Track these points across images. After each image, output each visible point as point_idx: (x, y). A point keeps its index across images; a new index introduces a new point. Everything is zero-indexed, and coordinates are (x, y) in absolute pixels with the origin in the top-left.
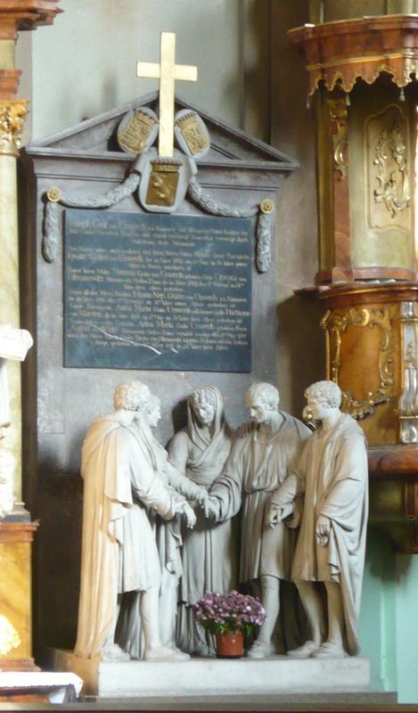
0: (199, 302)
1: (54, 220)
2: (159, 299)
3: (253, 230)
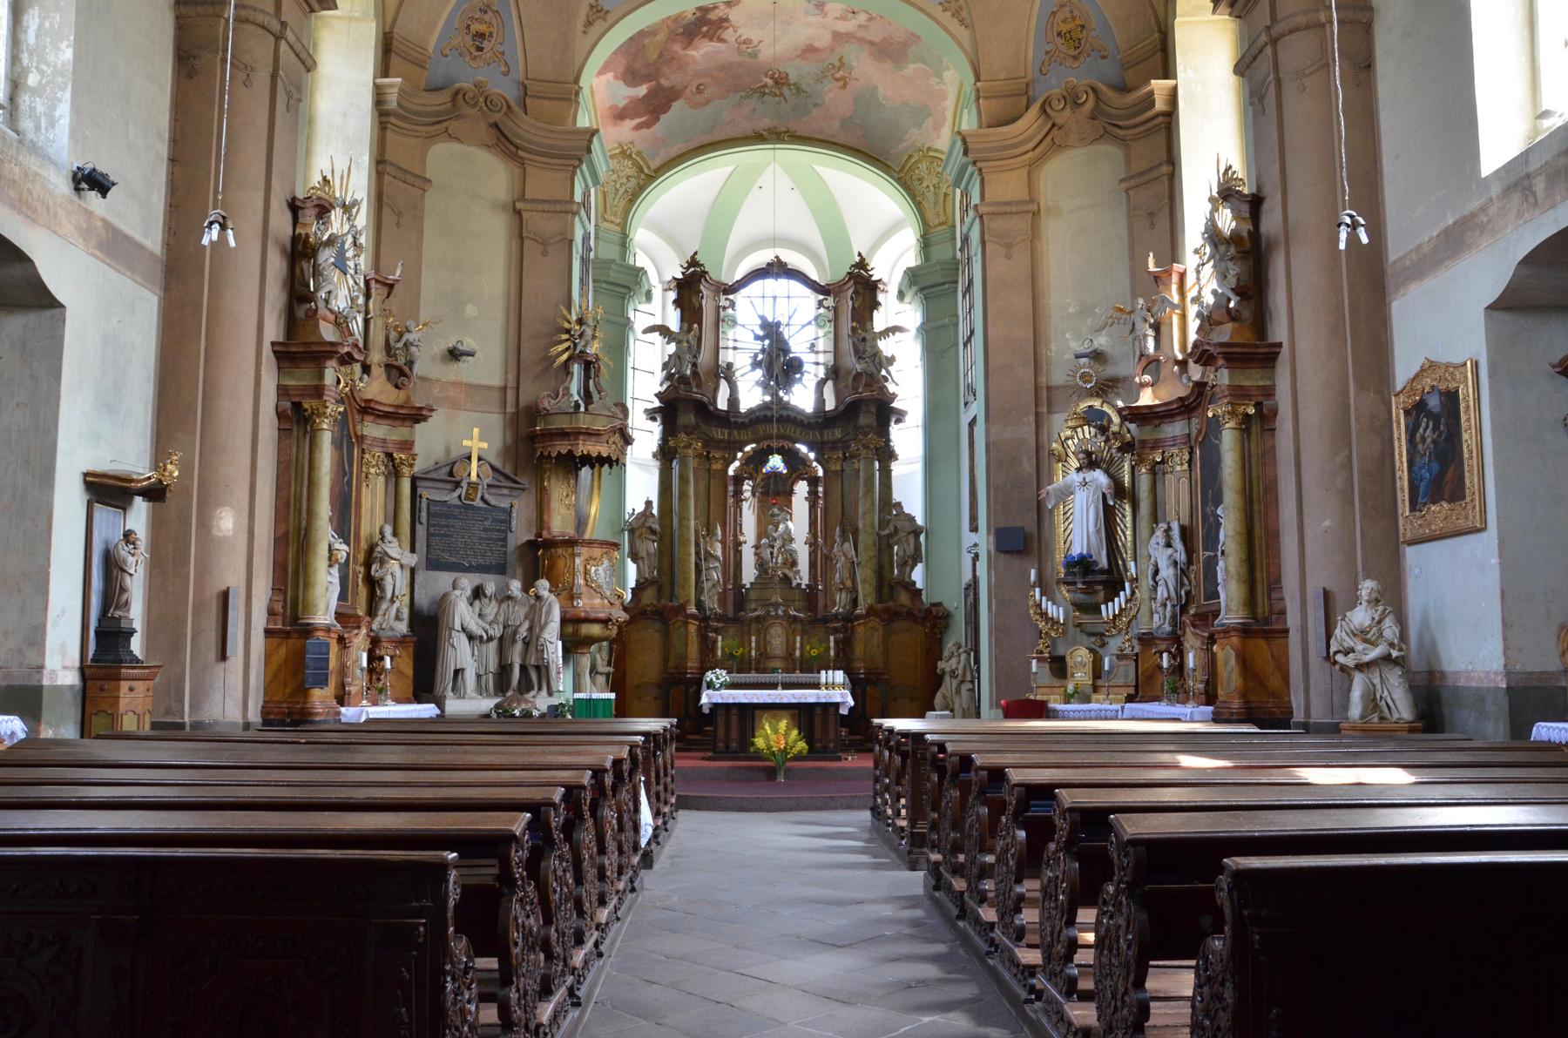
1: (424, 505)
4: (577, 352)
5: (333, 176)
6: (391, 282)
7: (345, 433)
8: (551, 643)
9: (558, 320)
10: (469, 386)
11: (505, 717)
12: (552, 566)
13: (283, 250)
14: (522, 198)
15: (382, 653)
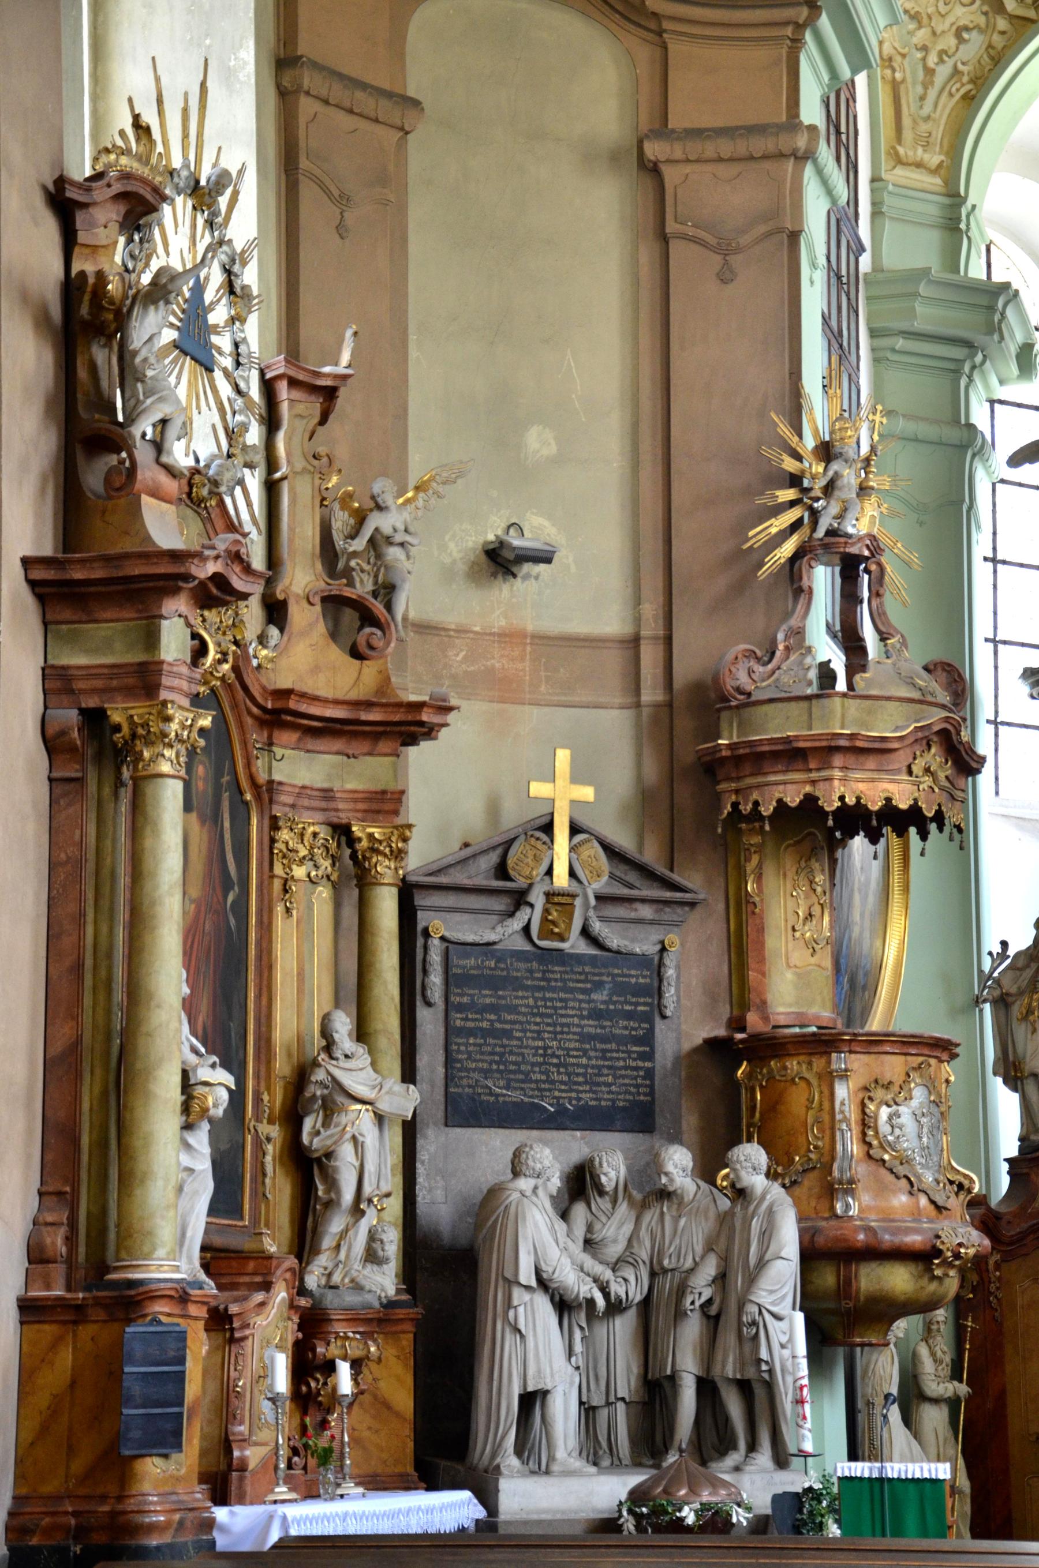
0: (596, 1050)
1: (435, 957)
2: (552, 1048)
3: (656, 968)
4: (820, 533)
5: (161, 112)
6: (328, 382)
7: (226, 779)
8: (778, 1318)
9: (766, 451)
10: (541, 639)
11: (658, 1529)
12: (774, 1107)
13: (42, 320)
14: (662, 129)
15: (334, 1350)
